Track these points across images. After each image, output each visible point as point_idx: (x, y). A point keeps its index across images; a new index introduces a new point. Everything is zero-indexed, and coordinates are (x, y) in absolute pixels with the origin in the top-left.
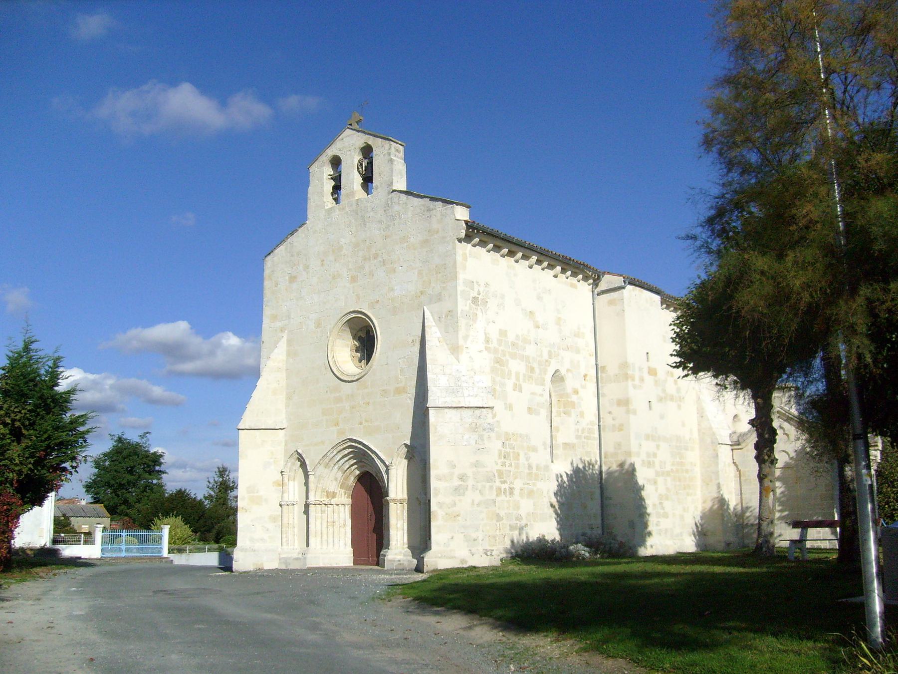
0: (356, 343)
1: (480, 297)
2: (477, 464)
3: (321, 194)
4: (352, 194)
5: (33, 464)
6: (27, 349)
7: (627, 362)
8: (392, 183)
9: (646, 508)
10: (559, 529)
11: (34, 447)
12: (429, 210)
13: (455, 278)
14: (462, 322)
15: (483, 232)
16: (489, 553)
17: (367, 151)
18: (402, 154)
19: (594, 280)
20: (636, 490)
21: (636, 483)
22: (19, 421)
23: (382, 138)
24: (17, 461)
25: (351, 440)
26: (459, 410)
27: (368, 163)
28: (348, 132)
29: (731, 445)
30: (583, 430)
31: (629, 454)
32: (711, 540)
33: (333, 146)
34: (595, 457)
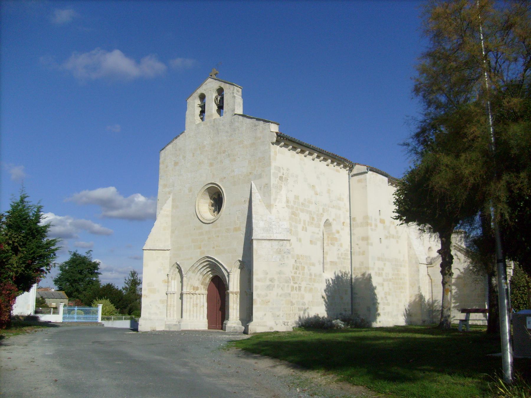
0: (212, 201)
1: (284, 176)
2: (280, 273)
3: (194, 115)
4: (211, 116)
5: (24, 268)
6: (22, 201)
7: (367, 216)
8: (234, 110)
9: (377, 300)
10: (327, 311)
11: (25, 257)
12: (255, 126)
13: (269, 165)
14: (273, 191)
15: (287, 139)
16: (286, 324)
17: (220, 91)
18: (240, 93)
19: (350, 168)
20: (372, 289)
21: (372, 285)
22: (17, 242)
23: (229, 84)
24: (15, 266)
25: (208, 257)
26: (270, 241)
27: (221, 98)
28: (210, 80)
29: (427, 265)
30: (342, 254)
31: (368, 268)
32: (414, 319)
33: (201, 88)
34: (348, 270)
